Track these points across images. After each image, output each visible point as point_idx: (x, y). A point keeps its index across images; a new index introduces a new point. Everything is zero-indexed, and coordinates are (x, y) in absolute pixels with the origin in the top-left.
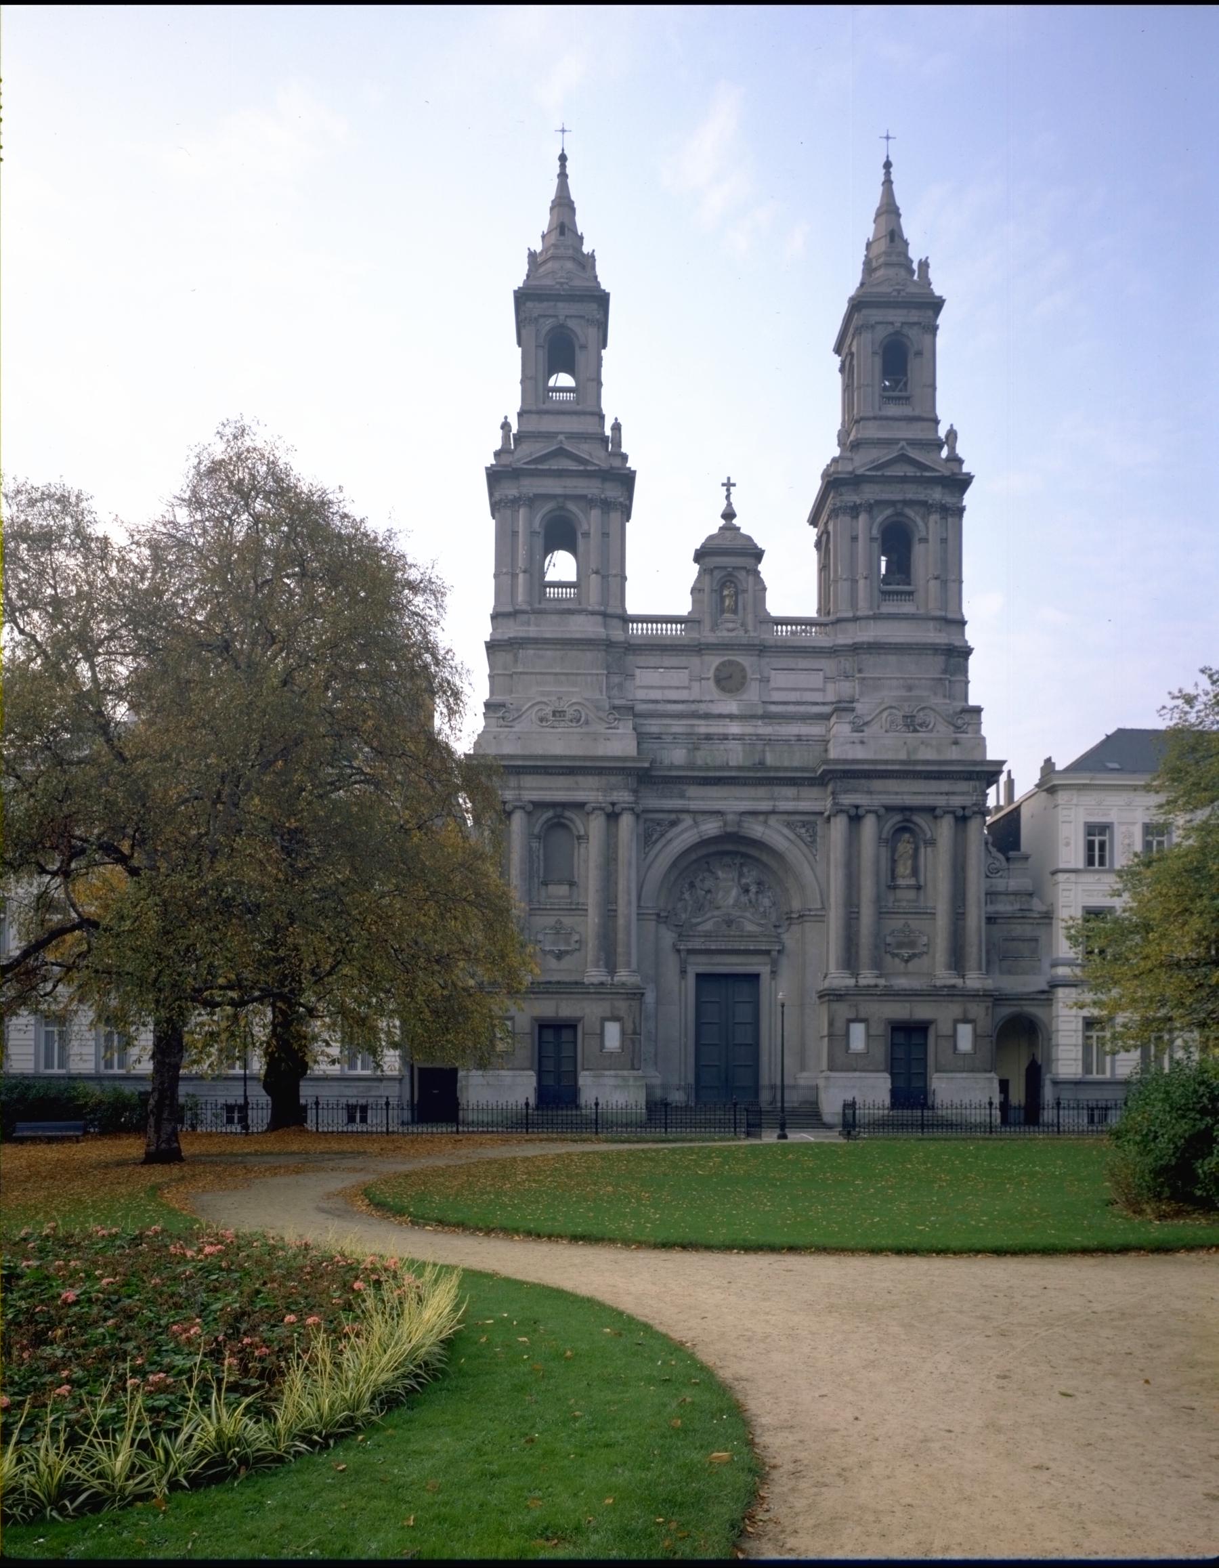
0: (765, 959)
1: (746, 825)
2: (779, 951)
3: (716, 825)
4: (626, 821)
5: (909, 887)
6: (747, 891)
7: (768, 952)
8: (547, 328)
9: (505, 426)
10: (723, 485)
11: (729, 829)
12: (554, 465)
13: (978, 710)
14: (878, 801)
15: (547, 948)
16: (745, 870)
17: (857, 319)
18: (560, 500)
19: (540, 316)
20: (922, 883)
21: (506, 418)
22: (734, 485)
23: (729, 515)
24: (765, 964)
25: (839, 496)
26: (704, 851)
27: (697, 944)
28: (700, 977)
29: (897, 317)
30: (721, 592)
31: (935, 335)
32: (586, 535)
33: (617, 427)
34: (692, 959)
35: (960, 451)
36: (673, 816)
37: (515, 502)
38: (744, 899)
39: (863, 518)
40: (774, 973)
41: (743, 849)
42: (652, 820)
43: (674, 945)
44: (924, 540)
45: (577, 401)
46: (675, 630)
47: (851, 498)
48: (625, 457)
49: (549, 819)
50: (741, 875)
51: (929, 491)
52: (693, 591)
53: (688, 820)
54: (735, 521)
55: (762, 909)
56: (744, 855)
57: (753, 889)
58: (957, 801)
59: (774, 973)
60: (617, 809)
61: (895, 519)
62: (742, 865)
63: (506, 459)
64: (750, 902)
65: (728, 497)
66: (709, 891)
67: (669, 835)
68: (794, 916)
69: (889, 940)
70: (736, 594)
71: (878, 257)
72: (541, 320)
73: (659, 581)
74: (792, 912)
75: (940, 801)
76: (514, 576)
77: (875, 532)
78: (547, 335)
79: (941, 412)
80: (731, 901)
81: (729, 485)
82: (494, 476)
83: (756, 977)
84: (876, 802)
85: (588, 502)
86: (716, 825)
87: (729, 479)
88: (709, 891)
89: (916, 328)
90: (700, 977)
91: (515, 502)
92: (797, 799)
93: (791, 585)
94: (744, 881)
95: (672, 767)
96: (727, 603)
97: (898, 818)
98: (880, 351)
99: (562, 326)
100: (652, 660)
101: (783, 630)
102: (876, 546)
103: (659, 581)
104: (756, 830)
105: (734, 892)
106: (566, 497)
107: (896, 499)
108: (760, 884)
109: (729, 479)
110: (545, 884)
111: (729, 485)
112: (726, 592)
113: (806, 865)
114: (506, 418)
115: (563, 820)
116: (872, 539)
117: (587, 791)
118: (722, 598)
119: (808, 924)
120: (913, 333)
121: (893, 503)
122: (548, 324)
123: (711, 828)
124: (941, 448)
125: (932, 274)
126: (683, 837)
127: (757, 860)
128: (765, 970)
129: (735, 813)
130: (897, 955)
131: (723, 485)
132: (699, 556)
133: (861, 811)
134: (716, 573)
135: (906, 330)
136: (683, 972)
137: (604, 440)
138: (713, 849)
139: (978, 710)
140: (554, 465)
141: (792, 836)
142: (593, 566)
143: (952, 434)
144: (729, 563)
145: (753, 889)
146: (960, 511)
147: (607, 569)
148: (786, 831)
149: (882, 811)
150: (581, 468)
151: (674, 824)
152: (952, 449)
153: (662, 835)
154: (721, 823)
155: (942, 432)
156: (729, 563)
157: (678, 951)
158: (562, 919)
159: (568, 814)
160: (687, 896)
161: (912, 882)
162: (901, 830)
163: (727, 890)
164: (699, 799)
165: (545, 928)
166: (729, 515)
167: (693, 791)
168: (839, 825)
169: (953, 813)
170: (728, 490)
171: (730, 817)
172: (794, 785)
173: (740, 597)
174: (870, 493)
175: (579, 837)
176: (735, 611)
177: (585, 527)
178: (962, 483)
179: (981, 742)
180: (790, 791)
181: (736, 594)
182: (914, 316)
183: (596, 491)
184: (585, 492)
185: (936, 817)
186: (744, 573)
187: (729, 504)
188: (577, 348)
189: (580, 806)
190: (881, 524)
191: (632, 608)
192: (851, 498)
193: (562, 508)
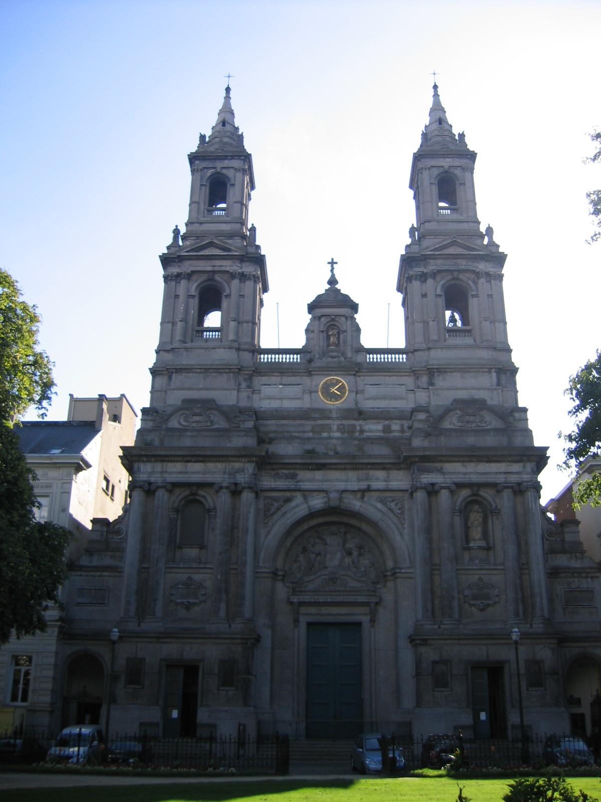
0: (365, 610)
1: (346, 501)
2: (377, 604)
3: (322, 501)
4: (247, 496)
5: (480, 548)
6: (350, 554)
7: (366, 604)
8: (209, 174)
9: (176, 231)
10: (329, 263)
11: (332, 504)
12: (452, 250)
13: (525, 410)
14: (449, 480)
15: (179, 601)
16: (348, 536)
17: (420, 165)
18: (211, 274)
19: (204, 168)
20: (491, 545)
21: (177, 226)
22: (336, 263)
23: (333, 281)
24: (366, 614)
25: (413, 268)
26: (314, 522)
27: (307, 598)
28: (310, 625)
29: (446, 163)
30: (327, 332)
31: (472, 173)
32: (228, 296)
33: (253, 229)
34: (303, 610)
35: (496, 239)
36: (288, 494)
37: (178, 276)
38: (347, 560)
39: (430, 281)
40: (373, 621)
41: (345, 520)
42: (271, 498)
43: (289, 599)
44: (476, 296)
45: (227, 215)
46: (296, 358)
47: (418, 270)
48: (498, 246)
49: (186, 497)
50: (345, 542)
51: (476, 264)
52: (307, 331)
53: (299, 498)
54: (337, 286)
55: (363, 569)
56: (352, 526)
57: (355, 553)
58: (514, 479)
59: (373, 621)
60: (239, 488)
61: (453, 282)
62: (345, 533)
63: (416, 248)
64: (353, 563)
65: (332, 270)
66: (319, 554)
67: (283, 510)
68: (389, 573)
69: (467, 592)
70: (338, 333)
71: (432, 132)
72: (206, 170)
73: (283, 325)
74: (386, 571)
75: (500, 479)
76: (174, 324)
77: (439, 291)
78: (209, 178)
79: (480, 216)
80: (336, 562)
81: (332, 263)
82: (166, 260)
83: (359, 624)
84: (448, 481)
85: (232, 276)
86: (265, 483)
87: (332, 259)
88: (319, 554)
89: (459, 169)
90: (310, 625)
91: (423, 278)
92: (398, 485)
93: (382, 325)
94: (348, 546)
95: (282, 457)
96: (332, 339)
97: (465, 493)
98: (436, 182)
99: (446, 172)
100: (274, 379)
101: (371, 358)
102: (441, 301)
103: (283, 325)
104: (356, 504)
105: (338, 555)
106: (214, 272)
107: (452, 267)
108: (360, 548)
109: (332, 259)
110: (180, 548)
111: (332, 263)
112: (330, 333)
113: (396, 532)
114: (177, 226)
115: (197, 497)
116: (438, 296)
117: (215, 472)
118: (328, 337)
119: (400, 580)
120: (458, 172)
121: (452, 271)
122: (209, 173)
123: (317, 502)
124: (483, 238)
125: (467, 140)
126: (298, 508)
127: (359, 529)
128: (365, 619)
129: (337, 491)
130: (473, 605)
131: (329, 263)
132: (312, 308)
133: (436, 488)
134: (322, 319)
135: (451, 170)
136: (296, 621)
137: (244, 237)
138: (321, 520)
139: (525, 410)
140: (206, 252)
141: (385, 509)
142: (233, 315)
143: (490, 230)
144: (333, 312)
145: (355, 553)
146: (500, 277)
147: (246, 320)
148: (379, 506)
149: (454, 487)
150: (226, 253)
151: (288, 500)
152: (491, 238)
153: (278, 509)
154: (326, 499)
155: (483, 229)
156: (333, 312)
157: (292, 603)
158: (193, 576)
159: (201, 492)
160: (301, 558)
161: (483, 544)
162: (469, 504)
163: (334, 553)
164: (309, 479)
165: (178, 584)
166: (333, 281)
167: (303, 474)
168: (420, 496)
169: (511, 487)
170: (332, 266)
171: (333, 495)
172: (384, 469)
173: (341, 336)
174: (432, 266)
175: (209, 511)
176: (338, 345)
177: (228, 291)
178: (500, 259)
179: (528, 433)
180: (381, 474)
181: (338, 333)
182: (457, 162)
183: (235, 268)
184: (228, 269)
185: (498, 491)
186: (343, 319)
187: (333, 276)
188: (229, 185)
189: (211, 485)
190: (443, 286)
191: (264, 345)
192: (418, 270)
193: (212, 279)
